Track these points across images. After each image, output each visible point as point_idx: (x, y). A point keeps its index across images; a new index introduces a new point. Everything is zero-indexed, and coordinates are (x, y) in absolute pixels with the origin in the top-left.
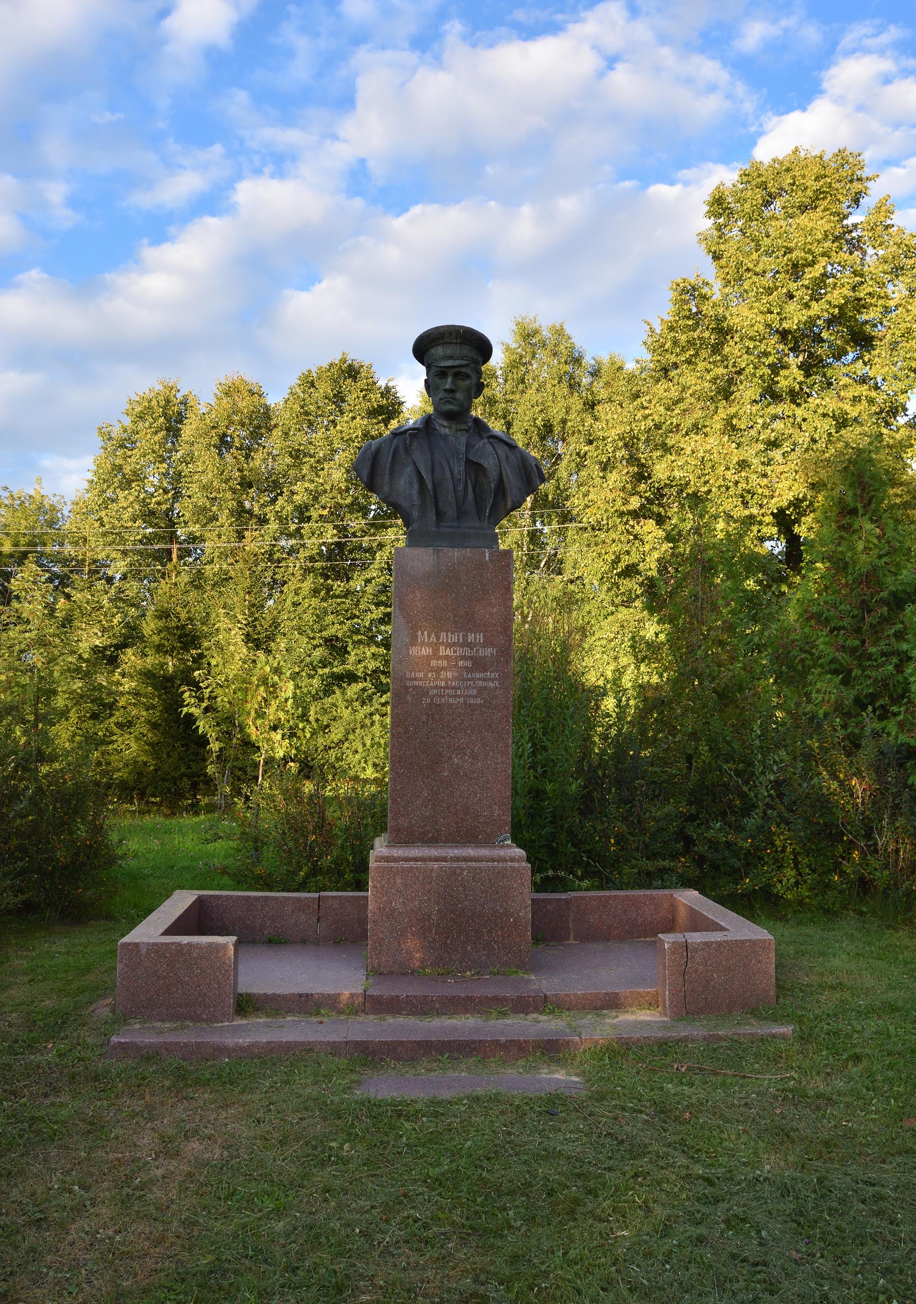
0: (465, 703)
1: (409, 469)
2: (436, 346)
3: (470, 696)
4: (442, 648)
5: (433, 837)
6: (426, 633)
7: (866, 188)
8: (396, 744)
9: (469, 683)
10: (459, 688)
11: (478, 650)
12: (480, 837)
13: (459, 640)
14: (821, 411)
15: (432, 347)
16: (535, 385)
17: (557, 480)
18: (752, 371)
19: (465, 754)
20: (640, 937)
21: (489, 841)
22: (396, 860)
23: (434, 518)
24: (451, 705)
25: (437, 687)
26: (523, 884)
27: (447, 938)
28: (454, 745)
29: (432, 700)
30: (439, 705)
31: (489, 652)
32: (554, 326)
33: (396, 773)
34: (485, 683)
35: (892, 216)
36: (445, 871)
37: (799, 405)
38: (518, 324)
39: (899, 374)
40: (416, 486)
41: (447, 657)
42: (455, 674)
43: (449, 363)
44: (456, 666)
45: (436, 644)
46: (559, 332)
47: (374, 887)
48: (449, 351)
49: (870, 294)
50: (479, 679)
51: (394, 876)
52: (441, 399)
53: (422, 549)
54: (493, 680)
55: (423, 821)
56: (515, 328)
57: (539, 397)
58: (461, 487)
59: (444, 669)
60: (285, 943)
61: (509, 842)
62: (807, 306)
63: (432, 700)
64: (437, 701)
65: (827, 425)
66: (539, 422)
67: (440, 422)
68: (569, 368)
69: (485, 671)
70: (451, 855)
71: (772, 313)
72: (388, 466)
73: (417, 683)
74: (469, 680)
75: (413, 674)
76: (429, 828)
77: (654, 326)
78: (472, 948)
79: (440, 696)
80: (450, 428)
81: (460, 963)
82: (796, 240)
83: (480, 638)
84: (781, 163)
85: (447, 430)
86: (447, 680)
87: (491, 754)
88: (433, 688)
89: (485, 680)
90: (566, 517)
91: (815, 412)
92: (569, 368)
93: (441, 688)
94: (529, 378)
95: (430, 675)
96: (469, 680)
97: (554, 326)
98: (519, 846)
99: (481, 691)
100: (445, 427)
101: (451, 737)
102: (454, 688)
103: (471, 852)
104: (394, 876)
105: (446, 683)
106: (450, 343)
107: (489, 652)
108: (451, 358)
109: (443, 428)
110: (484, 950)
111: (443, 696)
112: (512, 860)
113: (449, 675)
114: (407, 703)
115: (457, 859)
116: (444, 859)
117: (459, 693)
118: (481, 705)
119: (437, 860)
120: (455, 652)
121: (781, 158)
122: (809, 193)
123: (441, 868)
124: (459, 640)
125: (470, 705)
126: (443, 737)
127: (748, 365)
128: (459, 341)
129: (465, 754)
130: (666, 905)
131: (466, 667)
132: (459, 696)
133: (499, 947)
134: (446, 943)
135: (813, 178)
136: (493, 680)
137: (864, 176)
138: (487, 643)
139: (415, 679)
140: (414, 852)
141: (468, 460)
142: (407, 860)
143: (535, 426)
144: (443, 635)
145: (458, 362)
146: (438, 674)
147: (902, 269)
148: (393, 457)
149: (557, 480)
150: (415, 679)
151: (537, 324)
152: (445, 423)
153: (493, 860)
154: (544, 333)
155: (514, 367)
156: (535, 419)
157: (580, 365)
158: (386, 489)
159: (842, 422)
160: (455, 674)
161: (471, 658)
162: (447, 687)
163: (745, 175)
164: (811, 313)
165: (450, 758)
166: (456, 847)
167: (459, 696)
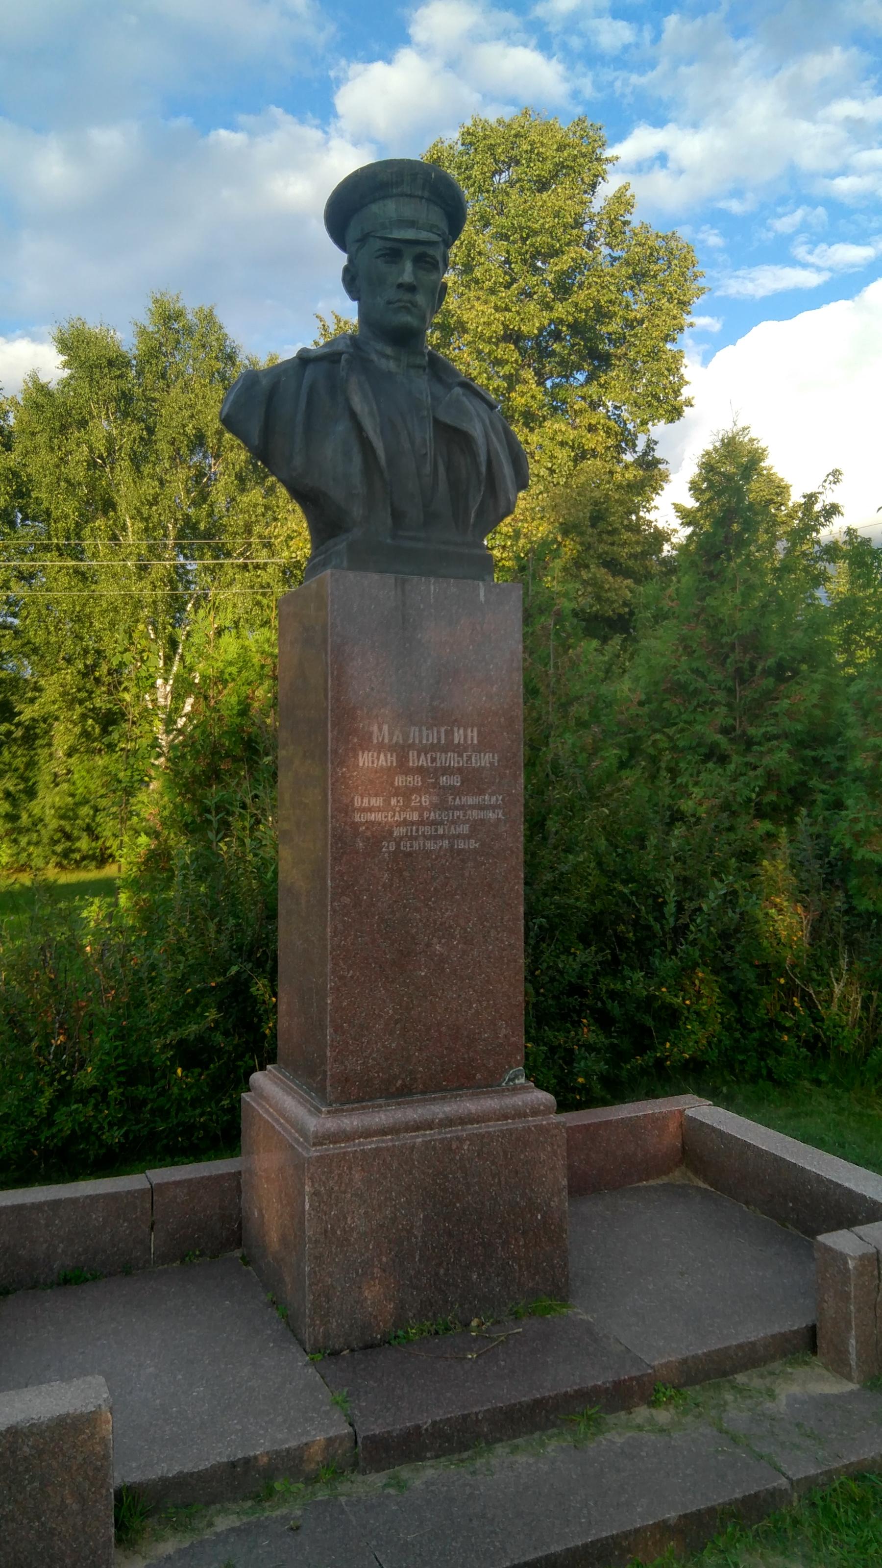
0: (452, 847)
1: (342, 427)
2: (385, 197)
3: (458, 836)
4: (413, 755)
5: (404, 1085)
6: (385, 727)
7: (605, 171)
8: (340, 926)
9: (457, 813)
10: (441, 823)
11: (469, 758)
12: (478, 1076)
13: (439, 739)
14: (559, 438)
15: (374, 201)
16: (180, 383)
17: (211, 506)
18: (485, 382)
19: (453, 937)
20: (641, 1180)
21: (490, 1083)
22: (348, 1136)
23: (389, 521)
24: (428, 853)
25: (405, 823)
26: (555, 1153)
27: (440, 1264)
28: (435, 922)
29: (398, 845)
30: (410, 854)
31: (486, 760)
32: (201, 310)
33: (342, 978)
34: (481, 815)
35: (632, 210)
36: (434, 1148)
37: (532, 430)
38: (156, 301)
39: (640, 401)
40: (357, 460)
41: (420, 770)
42: (435, 799)
43: (409, 234)
44: (435, 785)
45: (403, 747)
46: (209, 318)
47: (316, 1194)
48: (408, 210)
49: (610, 301)
50: (472, 807)
51: (350, 1168)
52: (389, 303)
53: (376, 577)
54: (493, 808)
55: (386, 1060)
56: (152, 306)
57: (184, 399)
58: (428, 469)
59: (415, 790)
60: (95, 1278)
61: (522, 1080)
62: (549, 307)
63: (398, 845)
64: (406, 846)
65: (563, 455)
66: (190, 429)
67: (379, 346)
68: (220, 365)
69: (481, 792)
70: (441, 1116)
71: (510, 310)
72: (300, 418)
73: (372, 817)
74: (457, 808)
75: (366, 800)
76: (396, 1070)
77: (327, 324)
78: (479, 1275)
79: (412, 838)
80: (397, 359)
81: (460, 1306)
82: (542, 221)
83: (473, 736)
84: (509, 126)
85: (392, 365)
86: (421, 809)
87: (493, 933)
88: (399, 824)
89: (482, 808)
90: (221, 552)
91: (552, 439)
92: (220, 365)
93: (412, 823)
94: (171, 374)
95: (393, 801)
96: (457, 808)
97: (201, 310)
98: (539, 1086)
99: (476, 826)
100: (387, 357)
101: (431, 909)
102: (434, 823)
103: (469, 1106)
104: (350, 1168)
105: (421, 815)
106: (411, 196)
107: (486, 760)
108: (412, 224)
109: (385, 357)
110: (498, 1275)
111: (416, 838)
112: (535, 1112)
113: (425, 800)
114: (357, 852)
115: (449, 1122)
116: (429, 1125)
117: (441, 831)
118: (475, 851)
119: (417, 1127)
120: (433, 760)
121: (507, 120)
122: (549, 165)
123: (426, 1144)
124: (439, 739)
125: (460, 851)
126: (417, 910)
127: (480, 374)
128: (426, 194)
129: (453, 937)
130: (673, 1126)
131: (452, 787)
132: (442, 837)
133: (520, 1267)
134: (437, 1274)
135: (555, 147)
136: (493, 808)
137: (603, 157)
138: (483, 746)
139: (370, 810)
140: (383, 1117)
141: (436, 421)
142: (367, 1134)
143: (185, 434)
144: (414, 731)
145: (424, 235)
146: (407, 799)
147: (643, 275)
148: (309, 403)
149: (211, 506)
150: (370, 810)
151: (179, 305)
152: (389, 351)
153: (505, 1117)
154: (189, 317)
155: (151, 355)
156: (184, 426)
157: (234, 364)
158: (298, 461)
159: (581, 455)
160: (435, 799)
161: (460, 770)
162: (421, 823)
163: (469, 134)
164: (555, 315)
165: (428, 945)
166: (443, 1098)
167: (442, 837)
